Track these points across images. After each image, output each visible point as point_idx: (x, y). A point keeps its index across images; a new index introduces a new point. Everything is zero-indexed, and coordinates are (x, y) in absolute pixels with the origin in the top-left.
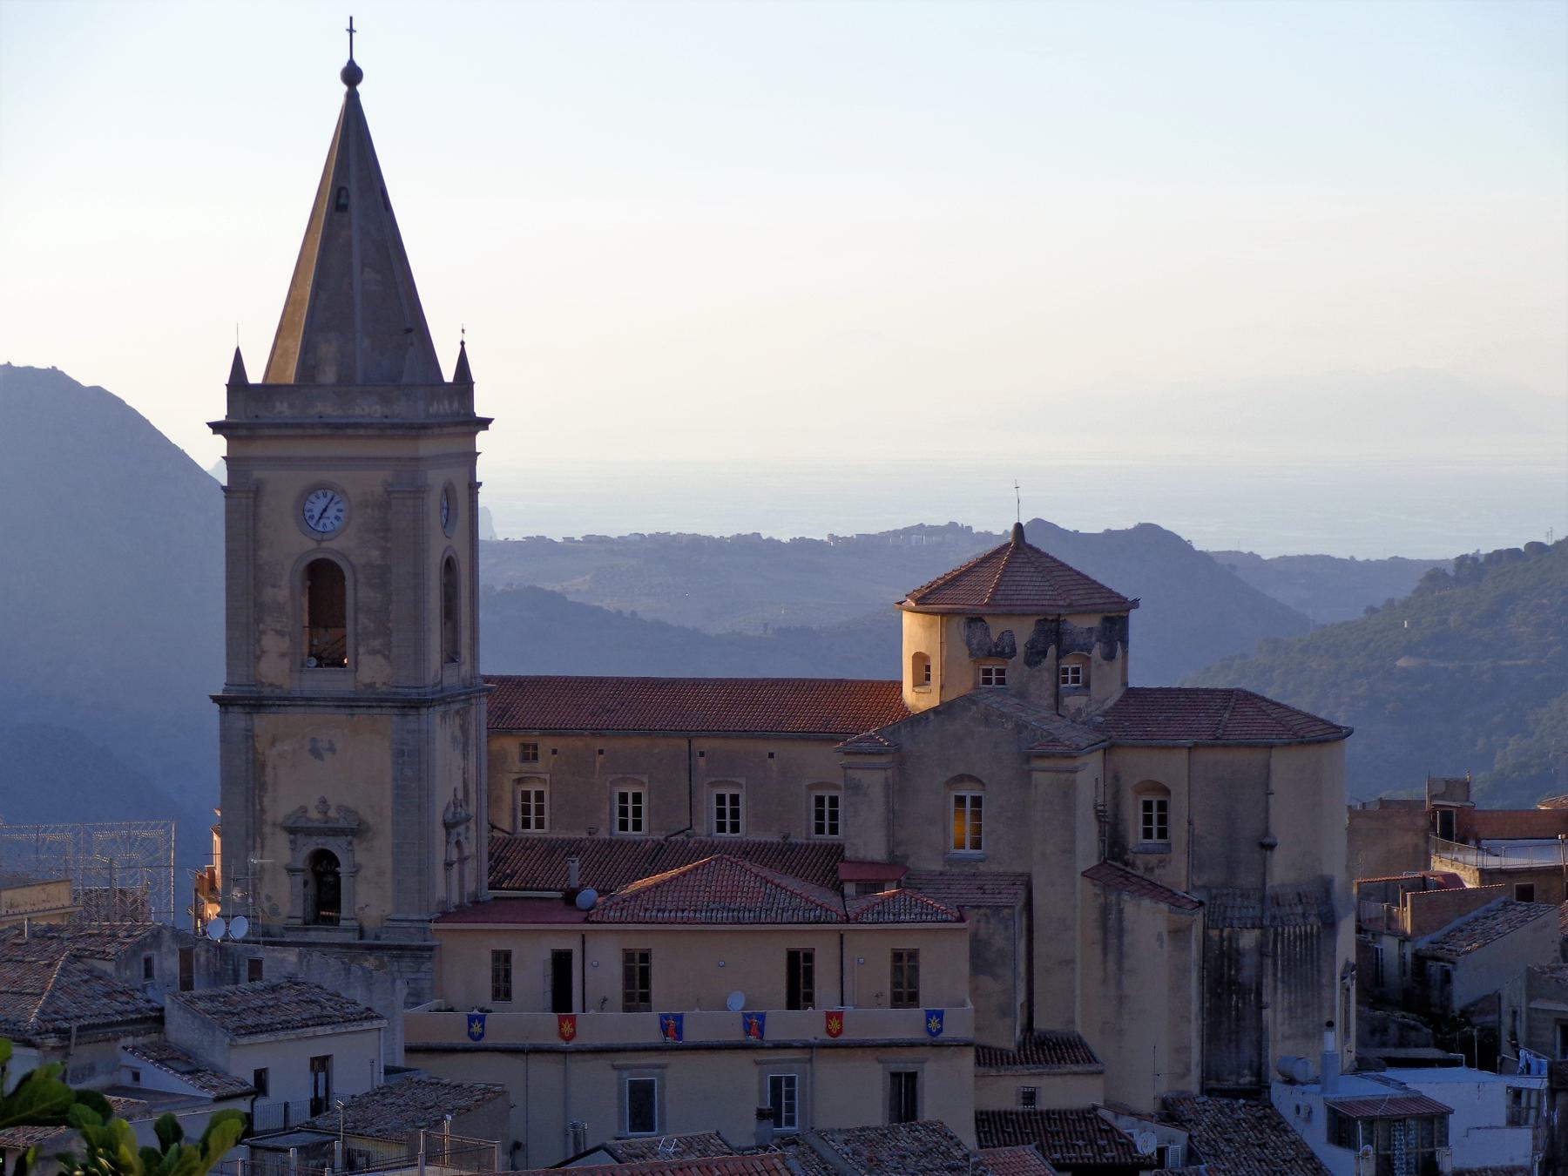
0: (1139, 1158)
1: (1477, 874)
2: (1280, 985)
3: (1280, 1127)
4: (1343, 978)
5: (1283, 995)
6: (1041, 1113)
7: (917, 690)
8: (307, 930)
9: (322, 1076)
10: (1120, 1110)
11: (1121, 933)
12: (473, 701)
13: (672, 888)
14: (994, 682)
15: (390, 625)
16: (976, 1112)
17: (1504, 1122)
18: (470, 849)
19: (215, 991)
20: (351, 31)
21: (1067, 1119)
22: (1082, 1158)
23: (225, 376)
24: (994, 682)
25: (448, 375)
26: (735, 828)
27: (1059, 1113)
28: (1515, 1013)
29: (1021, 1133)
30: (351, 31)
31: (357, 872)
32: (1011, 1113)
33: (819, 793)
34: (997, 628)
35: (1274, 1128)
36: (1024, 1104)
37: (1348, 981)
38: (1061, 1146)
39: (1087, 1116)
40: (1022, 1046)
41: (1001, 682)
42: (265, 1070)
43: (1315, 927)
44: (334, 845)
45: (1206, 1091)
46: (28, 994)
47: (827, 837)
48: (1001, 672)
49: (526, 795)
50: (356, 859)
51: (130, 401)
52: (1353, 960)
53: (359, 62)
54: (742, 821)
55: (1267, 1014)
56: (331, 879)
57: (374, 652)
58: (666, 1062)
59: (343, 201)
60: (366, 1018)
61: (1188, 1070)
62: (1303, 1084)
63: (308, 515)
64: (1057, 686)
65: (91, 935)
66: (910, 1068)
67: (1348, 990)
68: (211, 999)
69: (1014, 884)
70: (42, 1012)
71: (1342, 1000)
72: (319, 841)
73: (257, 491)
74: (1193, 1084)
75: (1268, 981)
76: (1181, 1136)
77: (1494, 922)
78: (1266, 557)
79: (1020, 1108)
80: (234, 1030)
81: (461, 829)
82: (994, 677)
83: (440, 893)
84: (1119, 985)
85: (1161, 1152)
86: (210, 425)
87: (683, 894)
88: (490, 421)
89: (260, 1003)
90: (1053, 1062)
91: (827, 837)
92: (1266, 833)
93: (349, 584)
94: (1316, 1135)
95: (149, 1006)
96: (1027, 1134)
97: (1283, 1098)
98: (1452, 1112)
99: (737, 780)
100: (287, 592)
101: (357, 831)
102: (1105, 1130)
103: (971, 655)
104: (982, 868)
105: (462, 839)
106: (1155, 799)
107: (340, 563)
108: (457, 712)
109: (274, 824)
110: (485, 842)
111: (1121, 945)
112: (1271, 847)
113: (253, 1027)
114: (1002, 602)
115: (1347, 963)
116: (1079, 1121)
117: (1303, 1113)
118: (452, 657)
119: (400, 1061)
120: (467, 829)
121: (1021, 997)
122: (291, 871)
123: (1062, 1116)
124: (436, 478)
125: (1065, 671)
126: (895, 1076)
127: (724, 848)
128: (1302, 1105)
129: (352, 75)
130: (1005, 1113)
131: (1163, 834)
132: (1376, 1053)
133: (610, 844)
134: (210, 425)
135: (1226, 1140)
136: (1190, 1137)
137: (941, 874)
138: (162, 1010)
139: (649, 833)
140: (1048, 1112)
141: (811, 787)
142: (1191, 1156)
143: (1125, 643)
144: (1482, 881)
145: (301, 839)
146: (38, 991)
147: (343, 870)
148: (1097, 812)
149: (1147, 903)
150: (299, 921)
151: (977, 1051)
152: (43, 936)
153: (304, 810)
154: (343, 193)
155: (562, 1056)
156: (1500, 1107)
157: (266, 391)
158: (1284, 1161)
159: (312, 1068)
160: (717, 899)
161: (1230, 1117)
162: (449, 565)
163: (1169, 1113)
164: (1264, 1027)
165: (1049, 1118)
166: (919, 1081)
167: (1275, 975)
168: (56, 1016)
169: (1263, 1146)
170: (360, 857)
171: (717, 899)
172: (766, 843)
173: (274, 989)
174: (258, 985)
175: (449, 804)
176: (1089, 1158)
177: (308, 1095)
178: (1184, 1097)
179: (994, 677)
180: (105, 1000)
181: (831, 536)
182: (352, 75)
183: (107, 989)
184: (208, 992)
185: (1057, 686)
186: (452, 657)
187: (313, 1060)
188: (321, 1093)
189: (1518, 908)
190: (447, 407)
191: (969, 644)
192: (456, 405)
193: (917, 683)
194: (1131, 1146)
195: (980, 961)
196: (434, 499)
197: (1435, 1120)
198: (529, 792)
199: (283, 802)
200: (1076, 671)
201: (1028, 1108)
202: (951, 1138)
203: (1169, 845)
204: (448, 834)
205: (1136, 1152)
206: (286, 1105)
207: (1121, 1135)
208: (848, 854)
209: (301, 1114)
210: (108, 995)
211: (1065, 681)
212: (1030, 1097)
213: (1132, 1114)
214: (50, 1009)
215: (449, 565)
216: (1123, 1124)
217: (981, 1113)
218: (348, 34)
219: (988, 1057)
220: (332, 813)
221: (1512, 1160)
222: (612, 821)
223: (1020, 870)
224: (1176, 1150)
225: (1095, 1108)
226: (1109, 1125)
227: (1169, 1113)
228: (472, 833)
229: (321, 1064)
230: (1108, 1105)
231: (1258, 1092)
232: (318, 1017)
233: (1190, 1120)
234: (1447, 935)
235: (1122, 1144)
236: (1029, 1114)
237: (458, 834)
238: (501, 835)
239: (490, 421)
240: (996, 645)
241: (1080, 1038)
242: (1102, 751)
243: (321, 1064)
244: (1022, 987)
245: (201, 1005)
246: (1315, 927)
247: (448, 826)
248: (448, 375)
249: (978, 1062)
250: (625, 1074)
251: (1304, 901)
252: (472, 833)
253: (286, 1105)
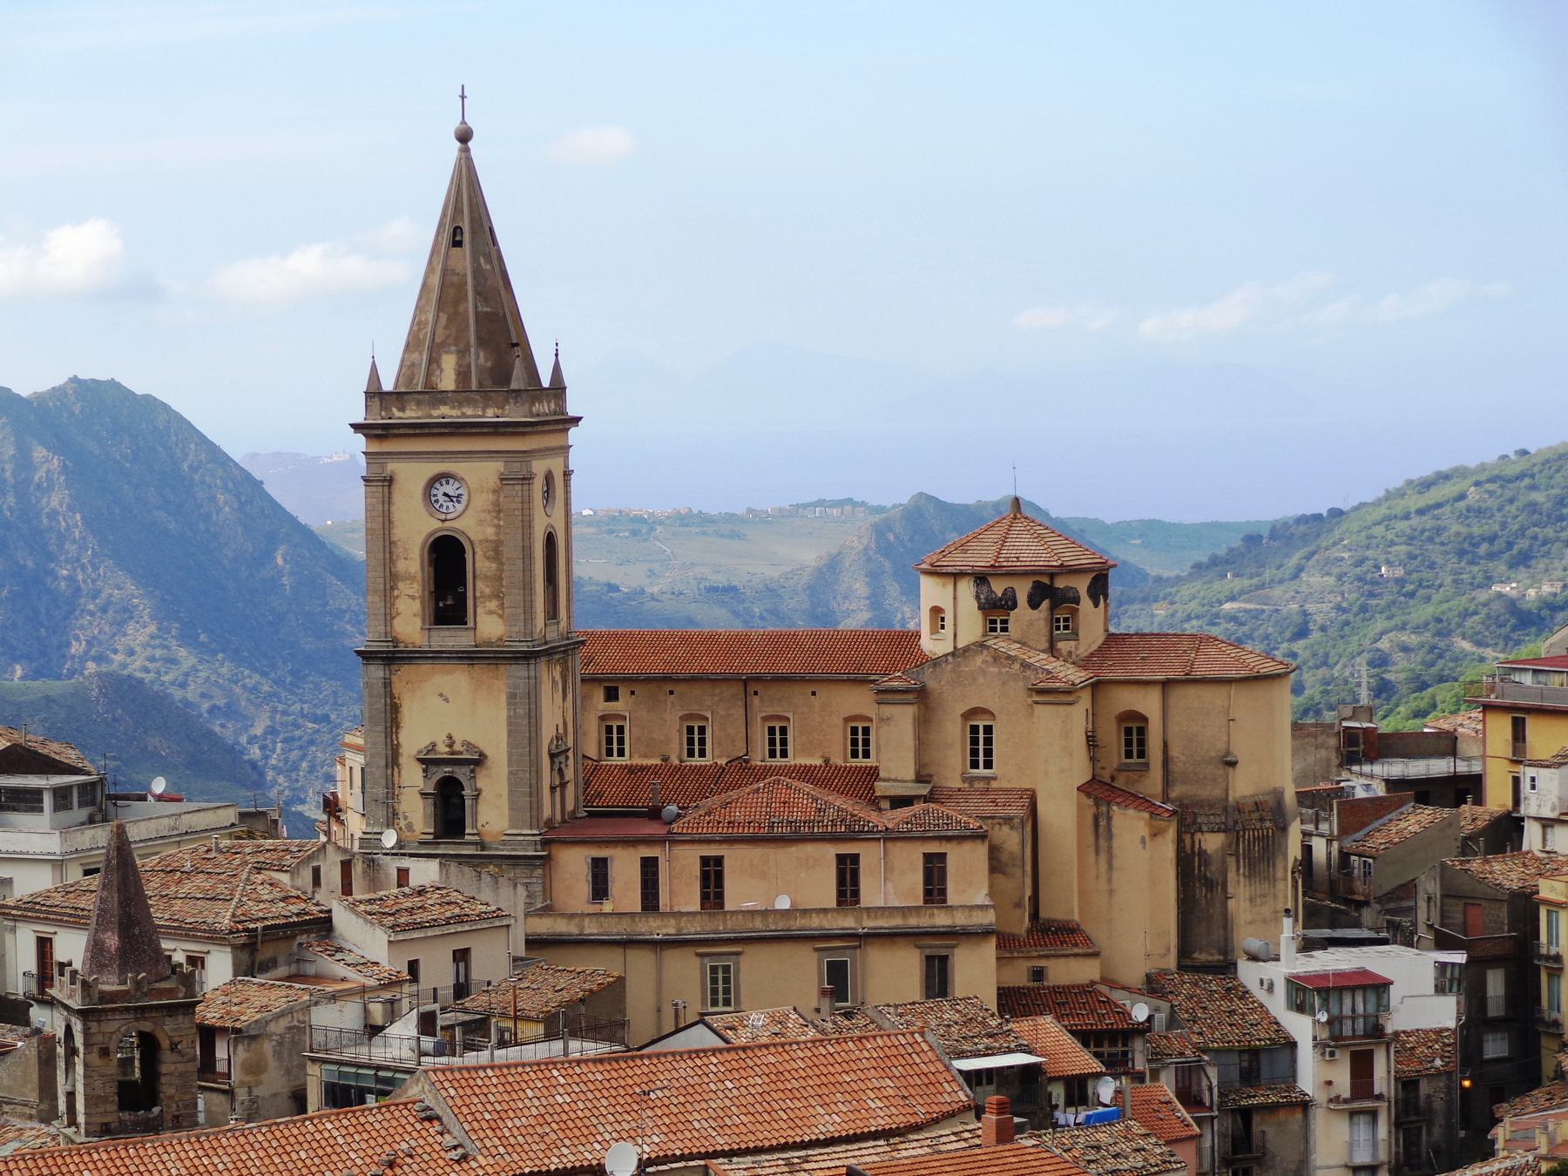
0: (1133, 1025)
1: (1383, 784)
2: (1242, 879)
3: (1245, 994)
4: (1293, 873)
5: (1245, 886)
6: (1048, 988)
7: (934, 637)
8: (439, 843)
9: (462, 965)
10: (1114, 985)
11: (1110, 837)
12: (570, 652)
13: (739, 804)
14: (999, 629)
15: (503, 590)
16: (998, 989)
17: (1432, 990)
18: (569, 774)
19: (373, 896)
20: (463, 97)
21: (1070, 992)
22: (1086, 1024)
23: (363, 385)
24: (999, 629)
25: (546, 383)
26: (784, 754)
27: (1063, 987)
28: (1429, 899)
29: (1034, 1005)
30: (463, 97)
31: (478, 795)
32: (1023, 988)
33: (854, 725)
34: (998, 587)
35: (1240, 998)
36: (1034, 981)
37: (1296, 875)
38: (1088, 1014)
39: (1087, 990)
40: (1030, 931)
41: (1005, 629)
42: (416, 961)
43: (1270, 831)
44: (461, 773)
45: (1182, 968)
46: (220, 900)
47: (860, 762)
48: (1005, 622)
49: (975, 729)
50: (908, 778)
51: (177, 406)
52: (1299, 858)
53: (470, 124)
54: (790, 748)
55: (1231, 903)
56: (456, 800)
57: (491, 612)
58: (739, 949)
59: (458, 238)
60: (497, 916)
61: (1169, 950)
62: (1264, 961)
63: (433, 499)
64: (1052, 633)
65: (268, 850)
66: (943, 952)
67: (1297, 882)
68: (370, 902)
69: (1021, 798)
70: (234, 915)
71: (1286, 891)
72: (447, 769)
73: (389, 481)
74: (1171, 962)
75: (1231, 876)
76: (1165, 1005)
77: (1407, 824)
78: (1108, 522)
79: (1031, 984)
80: (390, 928)
81: (562, 758)
82: (999, 626)
83: (547, 813)
84: (1110, 880)
85: (1150, 1019)
86: (352, 425)
87: (753, 810)
88: (579, 419)
89: (410, 905)
90: (1031, 946)
91: (860, 762)
92: (1228, 753)
93: (469, 556)
94: (1277, 1005)
95: (319, 908)
96: (1038, 1005)
97: (1249, 974)
98: (1392, 983)
99: (785, 714)
100: (413, 563)
101: (478, 761)
102: (1104, 1002)
103: (979, 608)
104: (994, 785)
105: (563, 766)
106: (1134, 725)
107: (462, 539)
108: (558, 660)
109: (409, 756)
110: (580, 769)
111: (1110, 848)
112: (1233, 764)
113: (407, 925)
114: (1005, 564)
115: (1296, 859)
116: (1080, 993)
117: (1266, 986)
118: (552, 613)
119: (522, 952)
120: (567, 758)
121: (1028, 893)
122: (424, 795)
123: (1066, 990)
124: (539, 467)
125: (1058, 620)
126: (929, 959)
127: (779, 771)
128: (1265, 978)
129: (464, 137)
130: (1019, 988)
131: (1141, 754)
132: (1315, 933)
133: (678, 769)
134: (352, 425)
135: (1201, 1008)
136: (1172, 1006)
137: (959, 790)
138: (330, 911)
139: (714, 757)
140: (1053, 987)
141: (847, 720)
142: (1172, 1022)
143: (1106, 597)
144: (1388, 790)
145: (433, 769)
146: (228, 898)
147: (467, 792)
148: (1088, 737)
149: (1131, 812)
150: (431, 837)
151: (998, 939)
152: (228, 852)
153: (434, 745)
154: (458, 230)
155: (620, 951)
156: (1429, 978)
157: (399, 397)
158: (1251, 1025)
159: (454, 960)
160: (777, 814)
161: (1205, 989)
162: (550, 540)
163: (1153, 986)
164: (1229, 917)
165: (1055, 992)
166: (949, 964)
167: (1238, 869)
168: (244, 918)
169: (1232, 1012)
170: (482, 782)
171: (777, 814)
172: (811, 766)
173: (421, 892)
174: (406, 890)
175: (552, 738)
176: (1092, 1025)
177: (451, 981)
178: (1164, 973)
179: (999, 626)
180: (282, 904)
181: (750, 510)
182: (464, 137)
183: (283, 894)
184: (367, 897)
185: (1052, 633)
186: (552, 613)
187: (454, 952)
188: (462, 980)
189: (1427, 812)
190: (546, 408)
191: (977, 597)
192: (553, 406)
193: (934, 631)
194: (1125, 1015)
195: (997, 864)
196: (538, 485)
197: (1380, 987)
198: (693, 727)
199: (413, 740)
200: (1066, 620)
201: (1036, 984)
202: (987, 1010)
203: (1147, 765)
204: (552, 763)
205: (1131, 1019)
206: (435, 990)
207: (1117, 1006)
208: (882, 774)
209: (447, 993)
210: (284, 899)
211: (1058, 628)
212: (1038, 974)
213: (1123, 988)
214: (239, 912)
215: (550, 540)
216: (1119, 997)
217: (1003, 988)
218: (460, 100)
219: (1007, 944)
220: (457, 747)
221: (1439, 1023)
222: (681, 749)
223: (1027, 786)
224: (1161, 1018)
225: (1093, 983)
226: (1106, 997)
227: (1153, 986)
228: (571, 762)
229: (461, 956)
230: (1104, 981)
231: (1226, 968)
232: (459, 916)
233: (1171, 992)
234: (1367, 835)
235: (1118, 1013)
236: (1038, 989)
237: (560, 763)
238: (590, 762)
239: (579, 419)
240: (1001, 599)
241: (1078, 925)
242: (1089, 689)
243: (461, 956)
244: (1028, 881)
245: (362, 907)
246: (1270, 831)
247: (552, 756)
248: (546, 383)
249: (999, 947)
250: (706, 960)
251: (1260, 808)
252: (571, 762)
253: (435, 990)
